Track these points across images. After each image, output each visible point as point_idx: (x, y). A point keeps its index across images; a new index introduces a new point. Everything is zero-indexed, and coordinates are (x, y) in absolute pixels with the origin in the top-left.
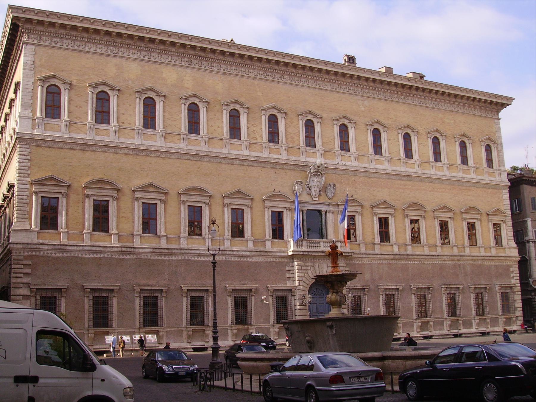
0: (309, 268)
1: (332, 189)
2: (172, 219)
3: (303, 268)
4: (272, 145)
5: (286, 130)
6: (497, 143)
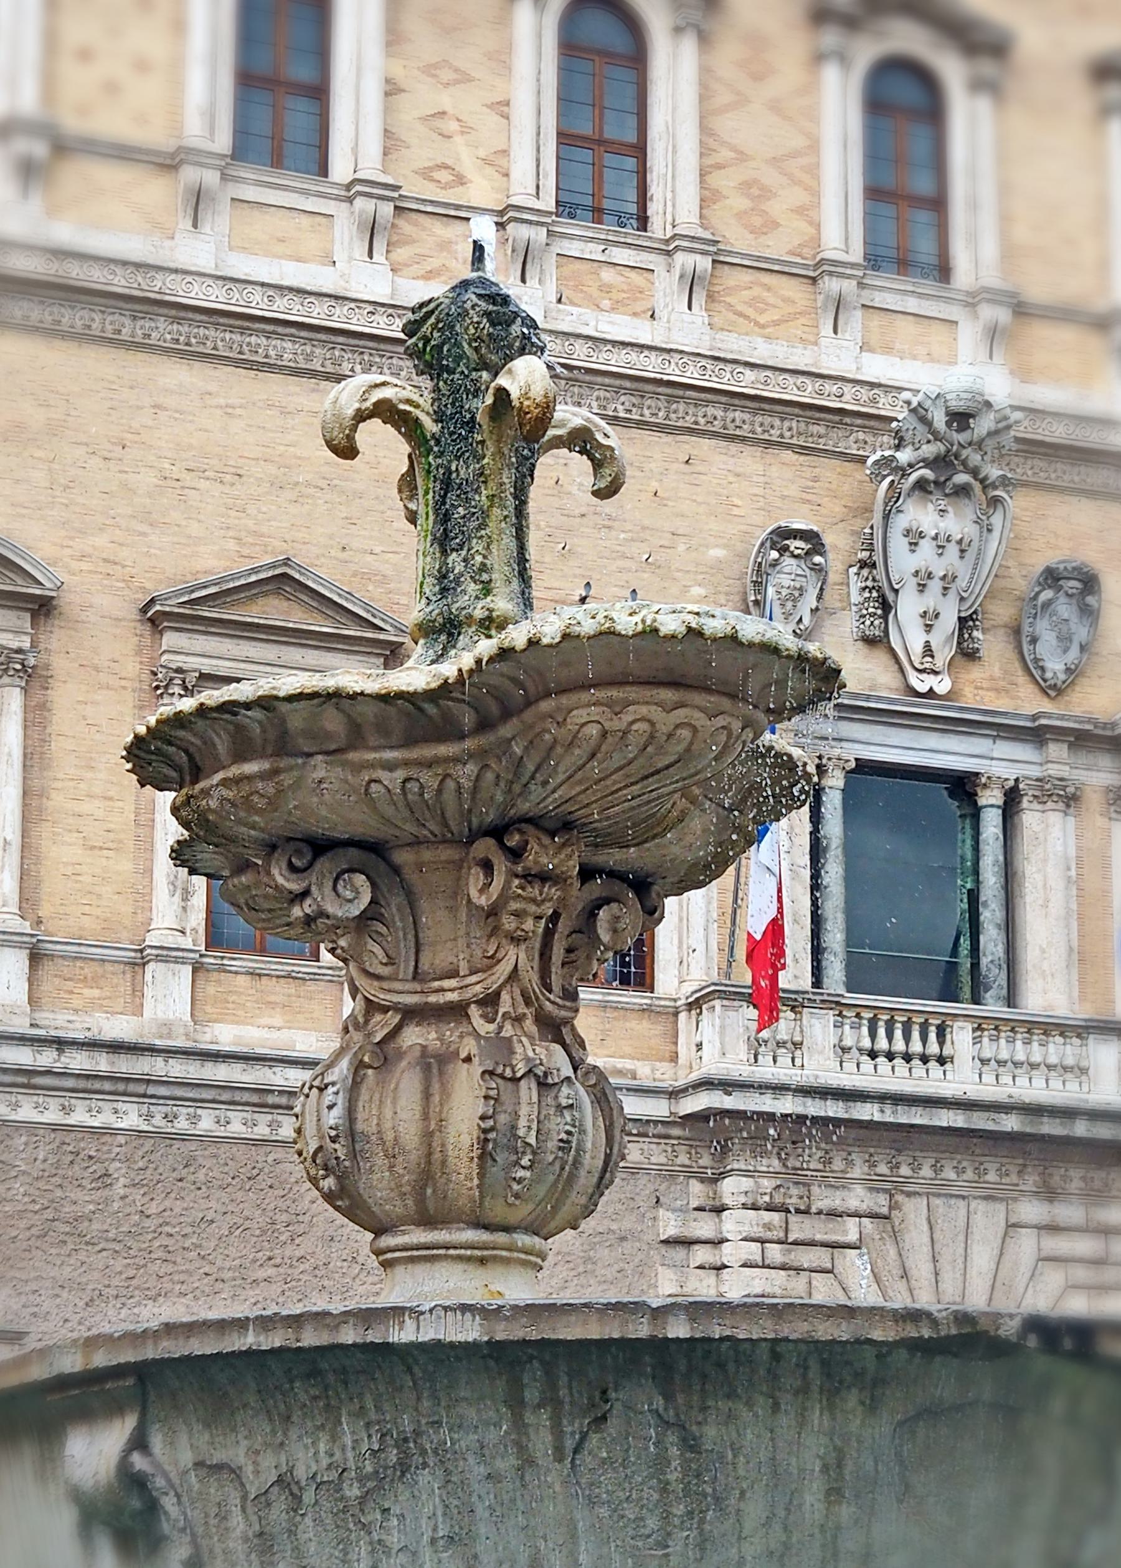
0: (851, 1230)
1: (1065, 609)
3: (800, 1228)
5: (705, 129)
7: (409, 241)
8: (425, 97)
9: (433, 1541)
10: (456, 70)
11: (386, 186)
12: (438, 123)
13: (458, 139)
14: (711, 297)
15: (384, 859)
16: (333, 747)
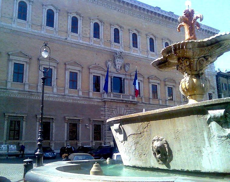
2: (33, 76)
4: (73, 34)
8: (85, 29)
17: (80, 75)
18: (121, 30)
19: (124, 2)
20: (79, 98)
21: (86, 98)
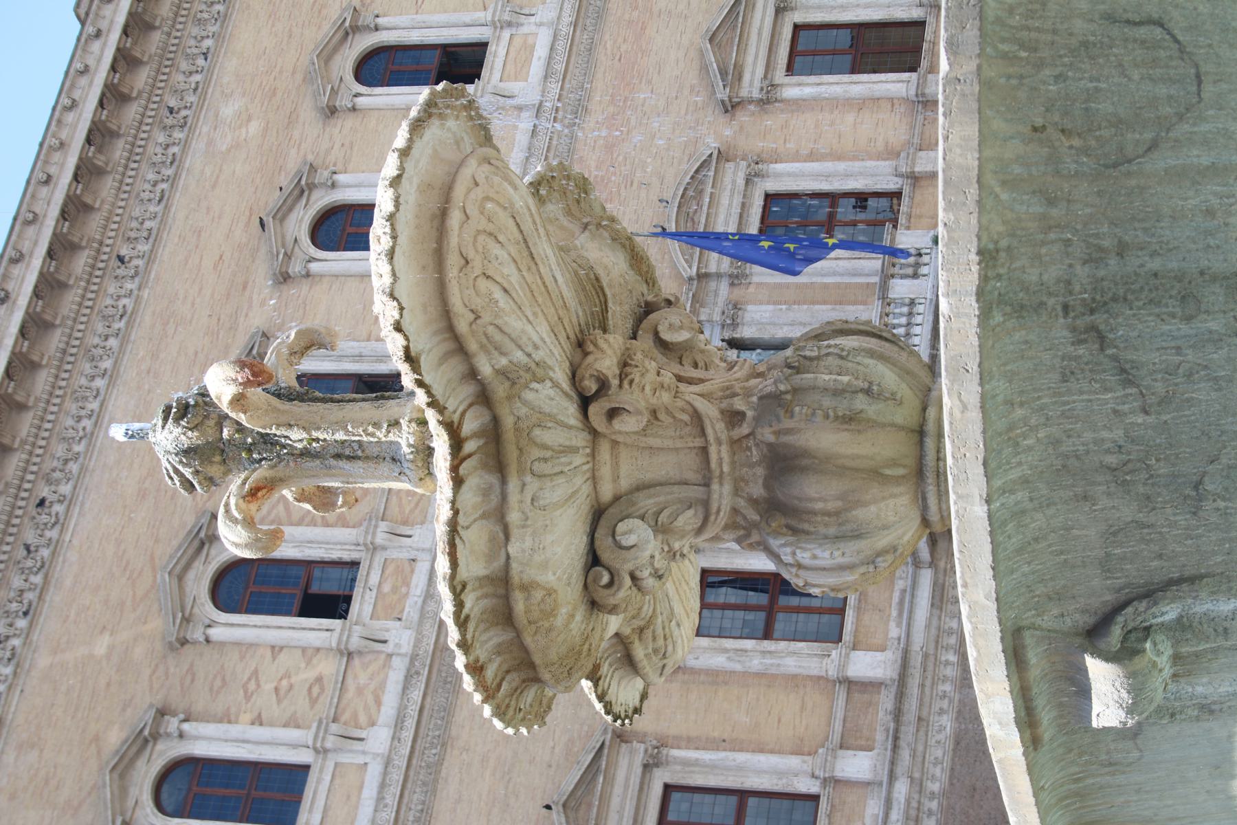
4: (361, 605)
6: (162, 713)
7: (355, 716)
8: (265, 700)
9: (1188, 319)
10: (250, 679)
11: (319, 728)
12: (282, 692)
13: (293, 680)
14: (405, 523)
15: (606, 509)
16: (501, 535)
17: (686, 763)
18: (334, 186)
19: (21, 365)
20: (901, 789)
21: (898, 714)
